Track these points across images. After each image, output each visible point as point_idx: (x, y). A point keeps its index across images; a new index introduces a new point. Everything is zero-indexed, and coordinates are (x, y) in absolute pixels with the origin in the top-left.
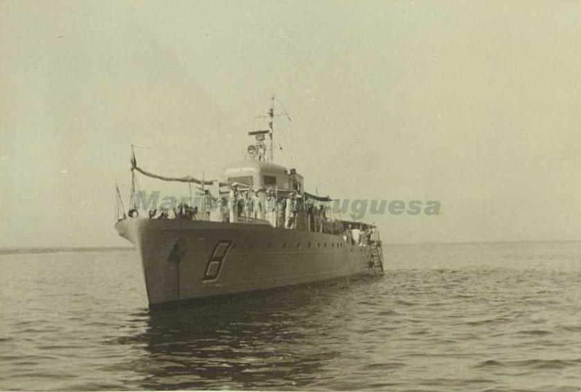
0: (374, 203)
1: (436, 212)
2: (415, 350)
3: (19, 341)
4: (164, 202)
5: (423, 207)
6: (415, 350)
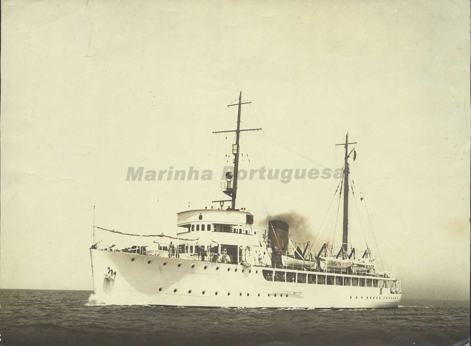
0: (298, 171)
1: (210, 178)
2: (210, 310)
3: (440, 315)
4: (204, 174)
5: (201, 174)
6: (210, 310)
